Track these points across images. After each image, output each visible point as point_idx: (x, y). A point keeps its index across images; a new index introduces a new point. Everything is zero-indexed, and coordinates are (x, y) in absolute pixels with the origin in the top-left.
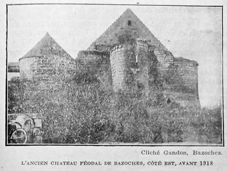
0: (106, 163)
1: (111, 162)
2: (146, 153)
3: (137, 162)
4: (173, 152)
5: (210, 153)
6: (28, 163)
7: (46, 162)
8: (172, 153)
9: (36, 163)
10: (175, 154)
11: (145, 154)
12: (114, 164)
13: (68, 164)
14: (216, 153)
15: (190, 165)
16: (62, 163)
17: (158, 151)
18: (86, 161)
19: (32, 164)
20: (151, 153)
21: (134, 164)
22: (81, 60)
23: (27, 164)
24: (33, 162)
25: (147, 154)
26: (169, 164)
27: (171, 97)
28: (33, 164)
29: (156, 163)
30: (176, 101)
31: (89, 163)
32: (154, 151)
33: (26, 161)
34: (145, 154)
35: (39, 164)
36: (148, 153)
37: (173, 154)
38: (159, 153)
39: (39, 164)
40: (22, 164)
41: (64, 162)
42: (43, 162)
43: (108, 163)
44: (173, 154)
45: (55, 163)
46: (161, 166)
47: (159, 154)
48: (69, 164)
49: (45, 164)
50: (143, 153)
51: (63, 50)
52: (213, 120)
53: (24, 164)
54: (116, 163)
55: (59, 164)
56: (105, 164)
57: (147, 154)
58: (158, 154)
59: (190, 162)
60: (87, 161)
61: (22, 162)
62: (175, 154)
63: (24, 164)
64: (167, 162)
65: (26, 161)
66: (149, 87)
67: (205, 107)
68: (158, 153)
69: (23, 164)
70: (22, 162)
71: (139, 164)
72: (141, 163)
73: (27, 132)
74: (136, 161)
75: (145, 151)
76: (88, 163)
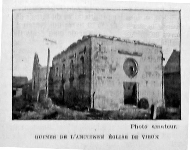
8: (155, 127)
33: (75, 135)
41: (80, 136)
62: (137, 128)
65: (75, 135)
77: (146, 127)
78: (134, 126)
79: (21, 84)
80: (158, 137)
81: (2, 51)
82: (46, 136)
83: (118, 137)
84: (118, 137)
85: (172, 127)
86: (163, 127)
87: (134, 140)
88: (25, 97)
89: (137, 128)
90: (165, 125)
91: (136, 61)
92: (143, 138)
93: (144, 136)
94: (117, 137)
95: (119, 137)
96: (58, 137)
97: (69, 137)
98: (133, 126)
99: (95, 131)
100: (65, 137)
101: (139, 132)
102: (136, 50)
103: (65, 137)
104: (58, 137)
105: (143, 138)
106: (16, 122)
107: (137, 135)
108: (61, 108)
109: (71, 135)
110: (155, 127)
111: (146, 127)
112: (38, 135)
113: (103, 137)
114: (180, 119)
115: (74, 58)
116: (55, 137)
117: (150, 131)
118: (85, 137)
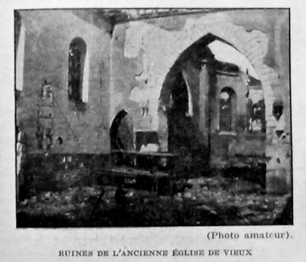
0: (100, 254)
3: (144, 251)
4: (279, 237)
6: (124, 252)
8: (250, 236)
9: (136, 253)
12: (113, 254)
13: (85, 254)
15: (128, 255)
18: (176, 250)
19: (130, 254)
21: (184, 252)
22: (64, 149)
26: (195, 254)
28: (132, 255)
30: (30, 153)
31: (181, 253)
33: (120, 251)
35: (141, 254)
37: (251, 237)
39: (141, 254)
40: (114, 255)
42: (147, 251)
43: (103, 253)
44: (251, 237)
49: (150, 255)
51: (285, 188)
53: (117, 255)
55: (229, 253)
56: (210, 254)
59: (129, 252)
61: (114, 252)
62: (223, 237)
63: (117, 255)
64: (238, 251)
65: (120, 251)
69: (116, 254)
70: (114, 252)
74: (143, 249)
76: (179, 253)
77: (237, 236)
78: (217, 234)
81: (31, 132)
85: (277, 236)
86: (263, 237)
89: (223, 237)
90: (265, 233)
91: (16, 175)
94: (187, 253)
95: (190, 254)
98: (215, 234)
100: (106, 253)
101: (216, 244)
103: (106, 253)
104: (95, 254)
105: (226, 254)
108: (217, 199)
110: (250, 236)
111: (237, 236)
112: (64, 249)
113: (91, 254)
114: (292, 224)
117: (241, 244)
118: (68, 253)
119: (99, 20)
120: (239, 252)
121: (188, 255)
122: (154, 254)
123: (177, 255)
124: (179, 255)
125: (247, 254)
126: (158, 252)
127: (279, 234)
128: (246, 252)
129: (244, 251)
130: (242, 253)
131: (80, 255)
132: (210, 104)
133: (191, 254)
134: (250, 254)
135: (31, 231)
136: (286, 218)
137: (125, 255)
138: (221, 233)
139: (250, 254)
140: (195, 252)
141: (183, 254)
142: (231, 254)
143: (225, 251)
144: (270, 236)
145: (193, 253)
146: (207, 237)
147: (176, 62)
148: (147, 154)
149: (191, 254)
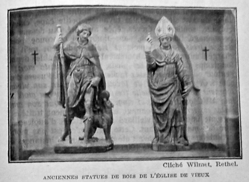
1: (118, 175)
2: (168, 166)
3: (198, 174)
5: (174, 165)
7: (64, 176)
9: (53, 178)
10: (178, 166)
11: (167, 166)
14: (232, 164)
16: (92, 177)
17: (181, 163)
18: (158, 174)
20: (174, 166)
23: (44, 179)
24: (50, 176)
25: (169, 167)
26: (75, 178)
27: (167, 78)
28: (50, 178)
29: (88, 177)
32: (176, 164)
33: (155, 174)
34: (167, 166)
36: (170, 166)
38: (182, 165)
41: (95, 176)
45: (55, 177)
46: (153, 178)
47: (182, 167)
48: (61, 179)
50: (165, 166)
52: (207, 127)
53: (153, 177)
54: (124, 176)
57: (169, 167)
58: (181, 166)
59: (48, 177)
60: (159, 173)
61: (151, 175)
62: (230, 165)
63: (153, 177)
64: (200, 174)
65: (155, 174)
66: (87, 29)
67: (49, 97)
68: (181, 165)
69: (152, 176)
70: (151, 175)
71: (103, 178)
72: (83, 178)
73: (32, 141)
75: (167, 164)
79: (22, 125)
80: (209, 175)
82: (68, 176)
83: (167, 175)
84: (167, 175)
87: (115, 179)
88: (226, 106)
89: (230, 165)
92: (193, 176)
93: (194, 174)
94: (166, 176)
96: (80, 178)
97: (149, 176)
99: (238, 165)
100: (117, 177)
102: (51, 106)
103: (117, 177)
105: (193, 176)
106: (20, 167)
107: (117, 174)
109: (150, 173)
115: (91, 83)
116: (77, 177)
119: (180, 105)
120: (201, 174)
121: (167, 177)
122: (65, 178)
123: (159, 177)
124: (160, 177)
125: (206, 176)
126: (68, 176)
127: (199, 166)
128: (205, 175)
129: (204, 174)
130: (203, 175)
131: (70, 178)
132: (185, 122)
133: (168, 177)
134: (208, 176)
135: (243, 157)
136: (241, 158)
137: (46, 179)
138: (229, 162)
139: (208, 176)
140: (133, 176)
141: (163, 177)
142: (196, 176)
143: (192, 174)
144: (222, 165)
145: (170, 176)
146: (163, 165)
147: (202, 115)
148: (89, 129)
149: (168, 177)
